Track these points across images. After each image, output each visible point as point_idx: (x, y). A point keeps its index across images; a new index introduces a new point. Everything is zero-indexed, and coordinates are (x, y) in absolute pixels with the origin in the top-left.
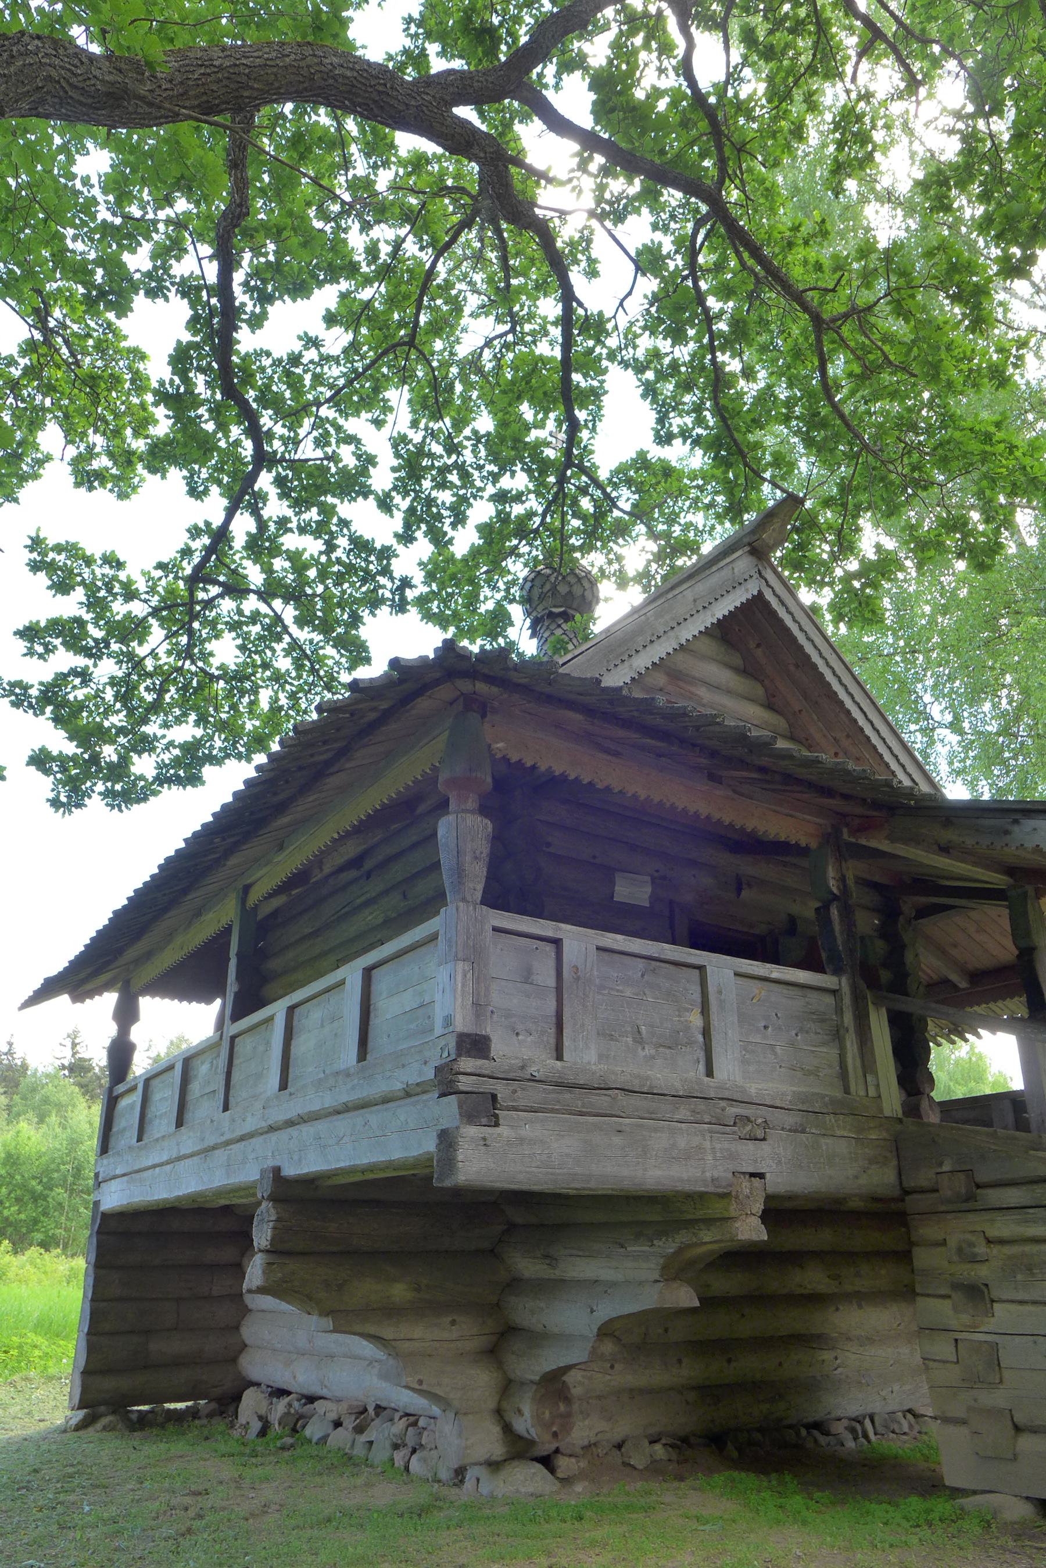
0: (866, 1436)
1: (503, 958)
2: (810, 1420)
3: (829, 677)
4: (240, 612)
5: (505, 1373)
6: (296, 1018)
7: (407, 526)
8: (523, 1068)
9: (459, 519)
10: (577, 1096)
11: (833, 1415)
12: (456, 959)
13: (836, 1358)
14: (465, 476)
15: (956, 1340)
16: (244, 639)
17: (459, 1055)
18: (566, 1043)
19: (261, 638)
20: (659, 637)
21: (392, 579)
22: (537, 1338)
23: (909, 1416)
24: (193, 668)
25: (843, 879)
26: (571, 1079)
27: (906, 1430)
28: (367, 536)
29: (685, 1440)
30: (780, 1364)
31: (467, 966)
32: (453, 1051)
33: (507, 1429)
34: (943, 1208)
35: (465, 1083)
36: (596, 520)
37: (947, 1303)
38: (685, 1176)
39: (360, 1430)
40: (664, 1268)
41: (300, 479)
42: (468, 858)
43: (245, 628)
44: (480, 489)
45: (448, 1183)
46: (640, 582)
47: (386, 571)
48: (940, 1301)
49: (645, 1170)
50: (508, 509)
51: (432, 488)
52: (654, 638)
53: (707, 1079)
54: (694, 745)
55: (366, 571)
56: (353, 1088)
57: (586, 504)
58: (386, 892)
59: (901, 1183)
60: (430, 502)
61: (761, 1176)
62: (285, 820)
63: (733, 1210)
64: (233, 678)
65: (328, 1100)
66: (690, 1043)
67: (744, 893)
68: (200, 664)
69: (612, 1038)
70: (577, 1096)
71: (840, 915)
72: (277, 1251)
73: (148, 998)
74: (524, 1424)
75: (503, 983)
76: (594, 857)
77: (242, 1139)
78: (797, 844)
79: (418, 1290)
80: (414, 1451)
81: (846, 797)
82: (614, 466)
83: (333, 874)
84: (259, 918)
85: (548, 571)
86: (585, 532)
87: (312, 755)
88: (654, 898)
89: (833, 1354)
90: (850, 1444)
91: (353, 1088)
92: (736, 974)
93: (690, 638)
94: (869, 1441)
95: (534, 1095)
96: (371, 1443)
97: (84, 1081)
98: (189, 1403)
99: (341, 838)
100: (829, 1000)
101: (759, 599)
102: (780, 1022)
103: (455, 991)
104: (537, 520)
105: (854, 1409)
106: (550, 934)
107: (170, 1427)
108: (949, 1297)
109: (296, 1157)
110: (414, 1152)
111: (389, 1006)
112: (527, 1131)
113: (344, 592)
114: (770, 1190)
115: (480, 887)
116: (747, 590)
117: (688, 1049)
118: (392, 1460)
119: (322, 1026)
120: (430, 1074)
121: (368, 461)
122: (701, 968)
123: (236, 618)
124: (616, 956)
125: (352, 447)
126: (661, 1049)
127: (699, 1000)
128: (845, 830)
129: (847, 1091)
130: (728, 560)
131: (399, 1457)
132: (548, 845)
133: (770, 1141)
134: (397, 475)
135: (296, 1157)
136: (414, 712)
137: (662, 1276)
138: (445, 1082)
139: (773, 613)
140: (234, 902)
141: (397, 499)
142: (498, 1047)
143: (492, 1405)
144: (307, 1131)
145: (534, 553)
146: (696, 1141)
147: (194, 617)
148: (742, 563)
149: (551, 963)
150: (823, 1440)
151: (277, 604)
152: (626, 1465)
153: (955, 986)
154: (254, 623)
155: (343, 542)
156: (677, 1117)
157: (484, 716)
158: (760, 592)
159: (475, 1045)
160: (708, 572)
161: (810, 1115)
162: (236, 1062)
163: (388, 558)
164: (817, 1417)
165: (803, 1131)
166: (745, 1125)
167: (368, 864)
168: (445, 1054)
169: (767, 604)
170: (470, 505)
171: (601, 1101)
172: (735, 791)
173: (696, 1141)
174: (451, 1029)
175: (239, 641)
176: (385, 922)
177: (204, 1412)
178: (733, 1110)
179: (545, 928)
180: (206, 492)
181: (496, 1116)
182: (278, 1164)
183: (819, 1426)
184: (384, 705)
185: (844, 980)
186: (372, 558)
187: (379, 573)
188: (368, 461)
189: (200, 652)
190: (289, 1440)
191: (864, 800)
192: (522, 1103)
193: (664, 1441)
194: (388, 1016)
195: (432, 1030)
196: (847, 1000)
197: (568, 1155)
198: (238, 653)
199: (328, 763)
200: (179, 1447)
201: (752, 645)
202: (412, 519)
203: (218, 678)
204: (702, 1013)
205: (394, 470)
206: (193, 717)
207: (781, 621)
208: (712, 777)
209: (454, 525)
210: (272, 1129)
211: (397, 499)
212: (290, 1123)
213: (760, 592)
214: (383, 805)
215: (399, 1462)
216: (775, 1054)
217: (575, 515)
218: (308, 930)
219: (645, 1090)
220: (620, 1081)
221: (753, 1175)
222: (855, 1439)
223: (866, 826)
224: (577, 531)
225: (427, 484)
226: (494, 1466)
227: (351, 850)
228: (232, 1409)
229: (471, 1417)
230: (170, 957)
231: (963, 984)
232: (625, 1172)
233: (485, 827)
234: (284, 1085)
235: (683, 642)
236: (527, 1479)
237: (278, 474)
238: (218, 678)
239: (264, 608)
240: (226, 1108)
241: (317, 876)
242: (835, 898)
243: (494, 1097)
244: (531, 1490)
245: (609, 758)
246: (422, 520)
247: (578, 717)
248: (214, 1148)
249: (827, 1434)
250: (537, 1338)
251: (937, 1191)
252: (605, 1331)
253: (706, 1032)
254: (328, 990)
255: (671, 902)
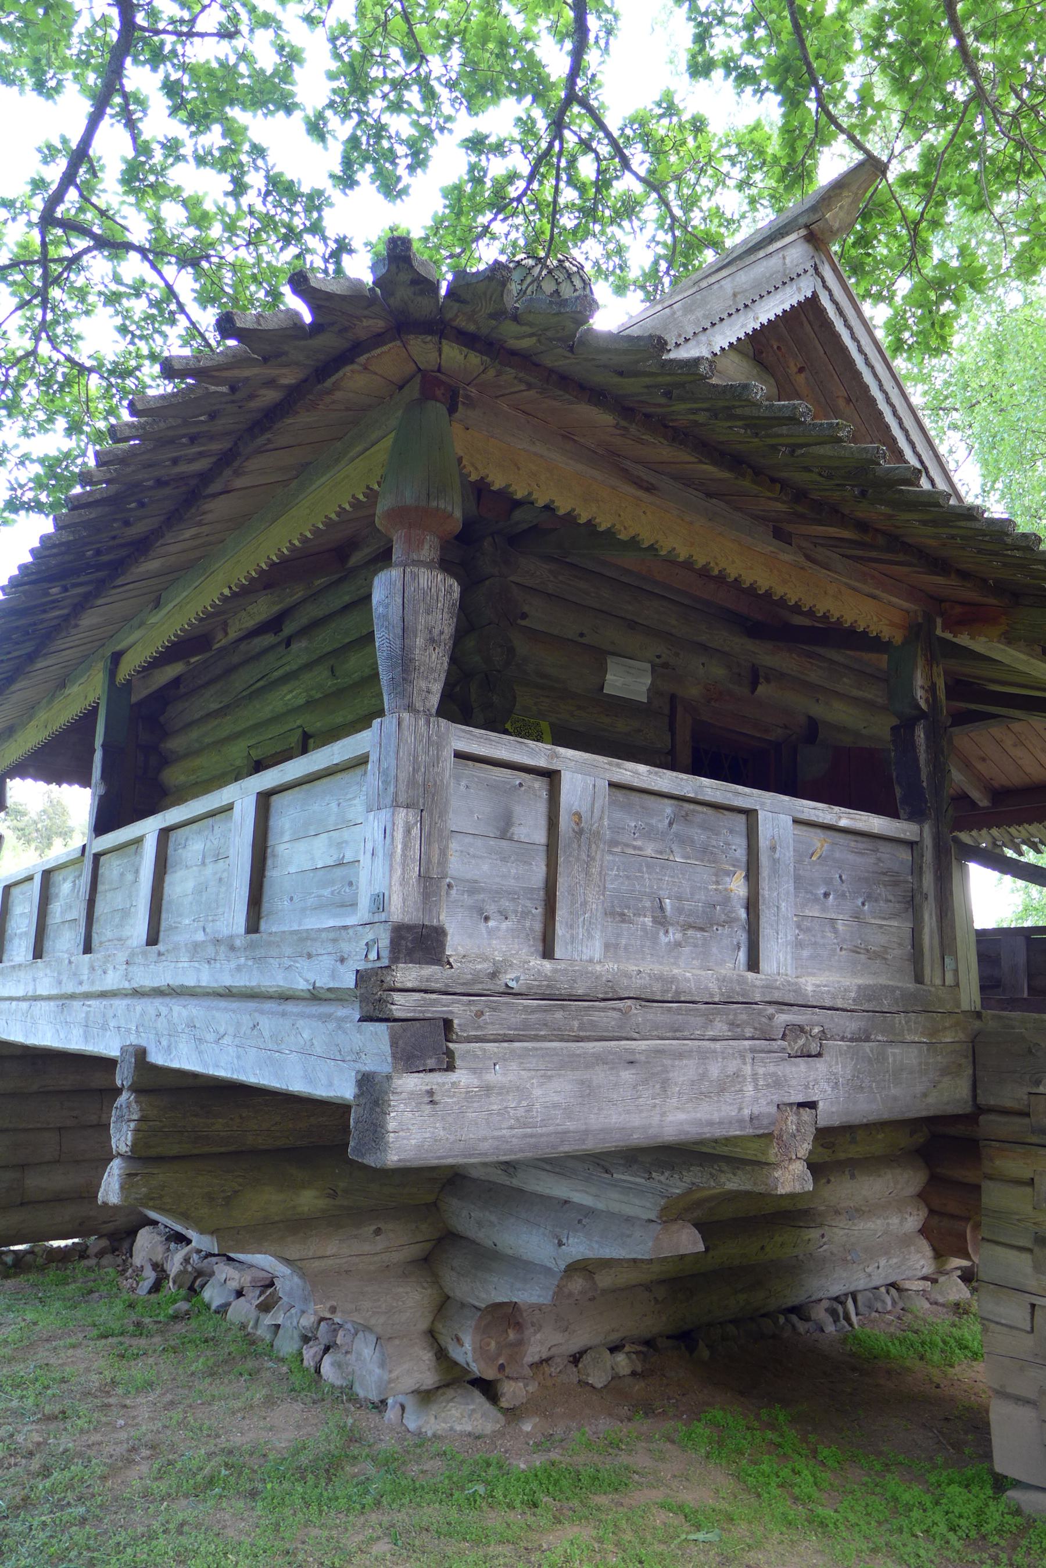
0: (847, 1318)
1: (467, 805)
2: (790, 1304)
3: (889, 418)
4: (117, 279)
5: (441, 1288)
6: (171, 845)
7: (347, 163)
8: (494, 975)
9: (419, 160)
10: (568, 1014)
11: (813, 1298)
12: (396, 805)
13: (823, 1236)
14: (429, 95)
15: (1033, 1306)
16: (125, 318)
17: (395, 959)
18: (560, 931)
19: (149, 318)
20: (687, 340)
21: (324, 239)
22: (487, 1258)
23: (893, 1291)
24: (56, 356)
25: (932, 689)
26: (564, 987)
27: (889, 1307)
28: (289, 176)
29: (649, 1343)
30: (763, 1248)
31: (412, 816)
32: (385, 954)
33: (441, 1355)
34: (1034, 1139)
35: (402, 1005)
36: (598, 191)
37: (1026, 1257)
38: (716, 1117)
39: (265, 1307)
40: (664, 1209)
41: (198, 89)
42: (420, 641)
43: (124, 301)
44: (449, 119)
45: (370, 1160)
46: (643, 287)
47: (316, 229)
48: (1015, 1253)
49: (663, 1114)
50: (484, 163)
51: (382, 111)
52: (681, 341)
53: (750, 975)
54: (773, 480)
55: (290, 228)
56: (239, 968)
57: (587, 168)
58: (308, 666)
59: (975, 1096)
60: (379, 130)
61: (812, 1105)
62: (151, 565)
63: (773, 1153)
64: (112, 372)
65: (204, 977)
66: (730, 922)
67: (761, 689)
68: (66, 350)
69: (623, 918)
70: (568, 1014)
71: (927, 738)
72: (142, 1157)
73: (17, 781)
74: (466, 1351)
75: (469, 839)
76: (582, 635)
77: (103, 995)
78: (877, 638)
79: (334, 1195)
80: (327, 1349)
81: (964, 575)
82: (629, 112)
83: (241, 640)
84: (134, 699)
85: (531, 262)
86: (581, 210)
87: (175, 461)
88: (653, 691)
89: (820, 1232)
90: (830, 1328)
91: (239, 968)
92: (796, 821)
93: (726, 346)
94: (851, 1325)
95: (514, 1014)
96: (278, 1326)
97: (20, 825)
98: (76, 1240)
99: (235, 595)
100: (905, 855)
101: (811, 305)
102: (844, 887)
103: (392, 855)
104: (521, 184)
105: (836, 1289)
106: (542, 763)
107: (52, 1274)
108: (1030, 1250)
109: (165, 1043)
110: (321, 1091)
111: (295, 856)
112: (495, 1077)
113: (259, 258)
114: (821, 1123)
115: (437, 688)
116: (799, 289)
117: (727, 930)
118: (301, 1354)
119: (203, 863)
120: (349, 981)
121: (291, 56)
122: (750, 814)
123: (114, 287)
124: (635, 797)
125: (270, 34)
126: (690, 932)
127: (744, 859)
128: (939, 621)
129: (919, 979)
130: (779, 244)
131: (309, 1354)
132: (524, 616)
133: (826, 1057)
134: (336, 84)
135: (165, 1043)
136: (338, 395)
137: (660, 1218)
138: (372, 997)
139: (829, 325)
140: (101, 674)
141: (333, 121)
142: (455, 945)
143: (423, 1325)
144: (180, 1011)
145: (514, 235)
146: (733, 1065)
147: (50, 280)
148: (795, 252)
149: (541, 808)
150: (802, 1327)
151: (170, 271)
152: (583, 1383)
153: (973, 804)
154: (138, 295)
155: (256, 180)
156: (710, 1033)
157: (452, 410)
158: (815, 295)
159: (420, 942)
160: (753, 258)
161: (875, 1016)
162: (100, 888)
163: (319, 209)
164: (790, 1302)
165: (867, 1040)
166: (798, 1037)
167: (289, 629)
168: (373, 956)
169: (822, 311)
170: (433, 141)
171: (606, 1017)
172: (808, 558)
173: (733, 1065)
174: (383, 917)
175: (118, 321)
176: (308, 702)
177: (93, 1250)
178: (783, 1018)
179: (537, 753)
180: (58, 89)
181: (450, 1054)
182: (144, 1044)
183: (799, 1311)
184: (289, 377)
185: (927, 828)
186: (298, 208)
187: (307, 230)
188: (291, 56)
189: (66, 333)
190: (183, 1306)
191: (985, 581)
192: (491, 1031)
193: (627, 1349)
194: (292, 870)
195: (354, 905)
196: (928, 856)
197: (555, 1106)
198: (117, 336)
199: (205, 478)
200: (45, 1319)
201: (793, 369)
202: (354, 156)
203: (90, 370)
204: (747, 877)
205: (332, 76)
206: (61, 423)
207: (837, 336)
208: (780, 535)
209: (411, 168)
210: (137, 993)
211: (333, 121)
212: (158, 993)
213: (815, 295)
214: (293, 549)
215: (309, 1361)
216: (835, 930)
217: (570, 182)
218: (214, 706)
219: (669, 996)
220: (636, 985)
221: (801, 1105)
222: (836, 1321)
223: (972, 617)
224: (570, 207)
225: (375, 104)
226: (425, 1397)
227: (262, 609)
228: (126, 1245)
229: (397, 1342)
230: (31, 737)
231: (984, 802)
232: (636, 1120)
233: (449, 592)
234: (153, 939)
235: (717, 350)
236: (464, 1417)
237: (167, 77)
238: (90, 370)
239: (151, 277)
240: (88, 949)
241: (221, 642)
242: (923, 715)
243: (448, 1024)
244: (469, 1428)
245: (640, 493)
246: (366, 159)
247: (605, 419)
248: (72, 997)
249: (806, 1319)
250: (487, 1258)
251: (1028, 1115)
252: (581, 1268)
253: (752, 905)
254: (212, 814)
255: (673, 698)
